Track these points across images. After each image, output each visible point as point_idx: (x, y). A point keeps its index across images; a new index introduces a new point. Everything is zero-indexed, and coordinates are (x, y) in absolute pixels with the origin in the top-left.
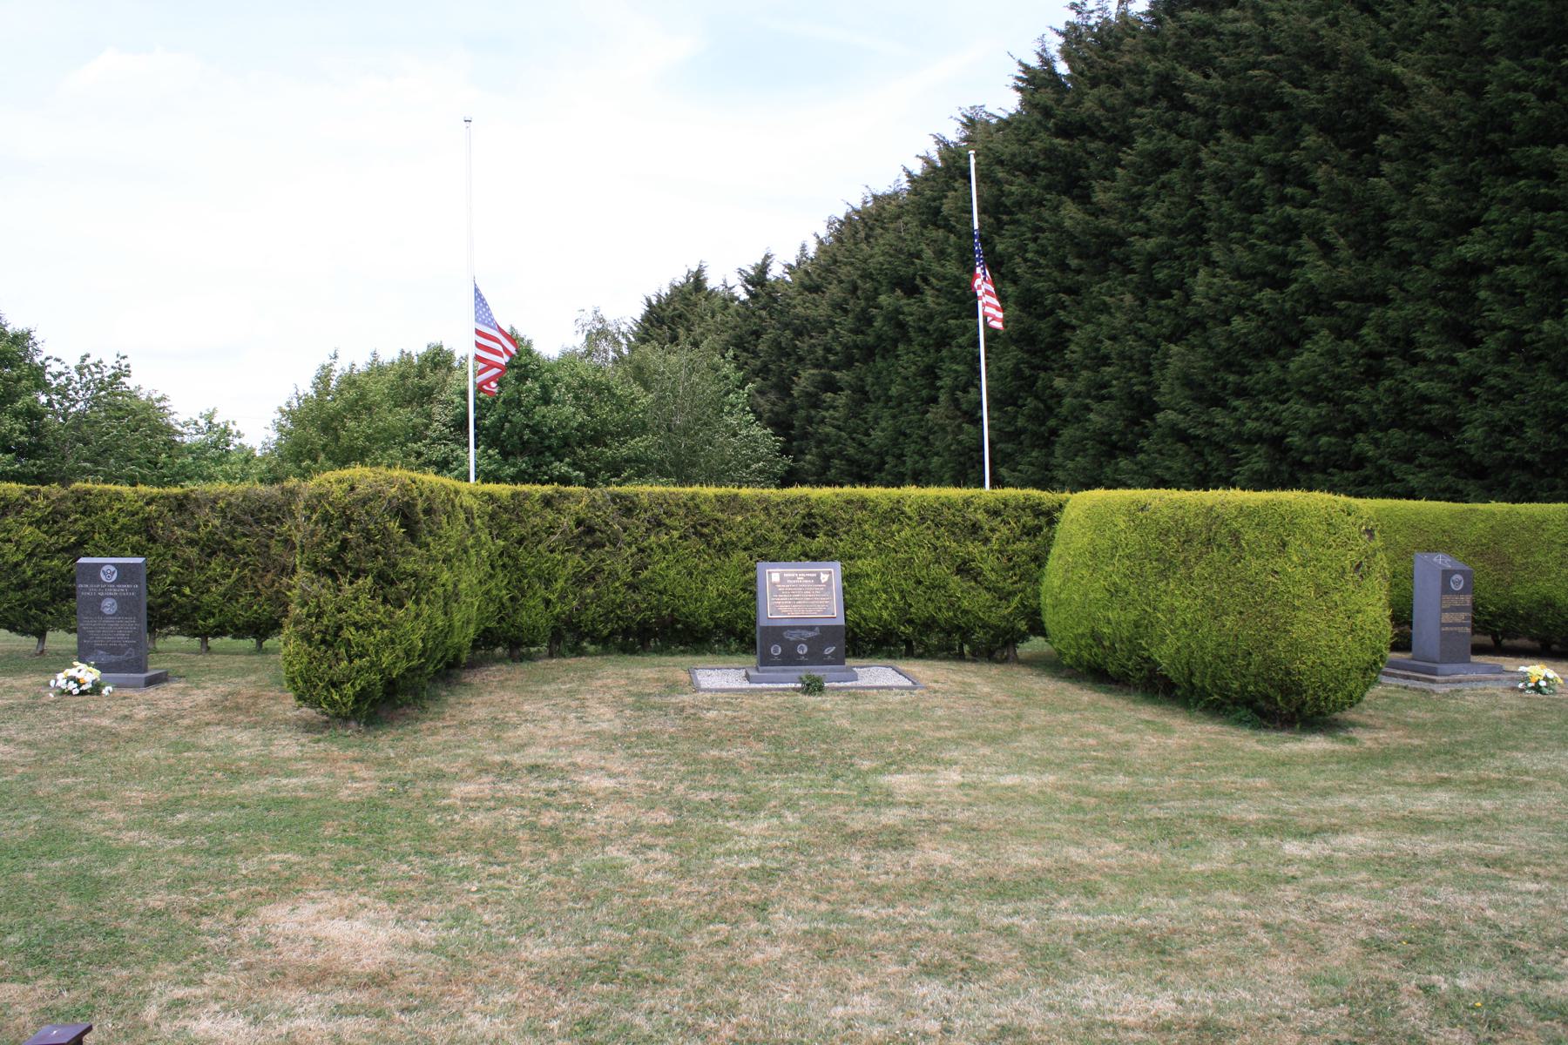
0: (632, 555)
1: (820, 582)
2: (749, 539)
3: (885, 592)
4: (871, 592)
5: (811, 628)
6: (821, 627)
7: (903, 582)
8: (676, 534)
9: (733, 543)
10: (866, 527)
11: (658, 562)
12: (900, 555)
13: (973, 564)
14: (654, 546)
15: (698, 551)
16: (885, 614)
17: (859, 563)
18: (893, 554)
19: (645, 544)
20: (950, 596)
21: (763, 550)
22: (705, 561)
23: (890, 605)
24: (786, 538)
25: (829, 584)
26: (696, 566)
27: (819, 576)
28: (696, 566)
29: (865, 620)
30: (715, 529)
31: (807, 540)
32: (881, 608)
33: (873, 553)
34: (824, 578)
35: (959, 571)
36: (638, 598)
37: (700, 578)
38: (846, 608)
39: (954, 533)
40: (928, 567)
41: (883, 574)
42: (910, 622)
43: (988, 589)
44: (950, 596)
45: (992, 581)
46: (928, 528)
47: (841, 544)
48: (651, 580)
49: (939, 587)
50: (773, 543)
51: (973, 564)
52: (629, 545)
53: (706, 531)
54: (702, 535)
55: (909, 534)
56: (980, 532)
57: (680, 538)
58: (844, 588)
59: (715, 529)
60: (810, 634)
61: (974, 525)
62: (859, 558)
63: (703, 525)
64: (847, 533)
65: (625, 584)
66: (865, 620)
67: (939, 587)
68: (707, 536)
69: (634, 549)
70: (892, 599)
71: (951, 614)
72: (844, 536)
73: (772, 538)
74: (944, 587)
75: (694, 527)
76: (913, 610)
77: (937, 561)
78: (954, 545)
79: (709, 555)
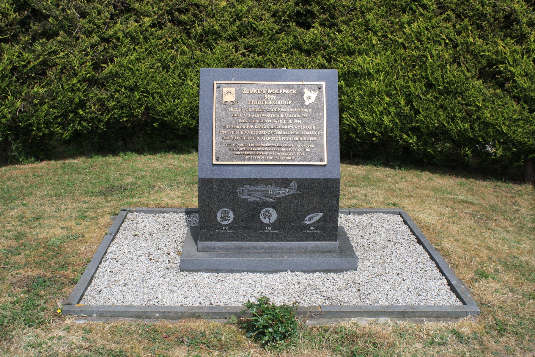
0: (92, 46)
1: (302, 105)
2: (234, 28)
3: (388, 95)
4: (372, 94)
5: (284, 183)
6: (302, 183)
7: (411, 84)
8: (147, 21)
9: (215, 33)
10: (370, 16)
11: (126, 54)
12: (409, 52)
13: (501, 67)
14: (120, 34)
15: (175, 41)
16: (386, 121)
17: (360, 59)
18: (402, 51)
19: (111, 32)
20: (468, 105)
21: (251, 41)
22: (183, 53)
23: (392, 109)
24: (277, 27)
25: (316, 107)
26: (173, 59)
27: (301, 93)
28: (173, 59)
29: (363, 124)
30: (195, 16)
31: (301, 30)
32: (381, 113)
33: (377, 48)
34: (310, 97)
35: (482, 75)
36: (103, 95)
37: (177, 72)
38: (342, 110)
39: (479, 27)
40: (442, 67)
41: (387, 73)
42: (415, 130)
43: (517, 99)
44: (468, 105)
45: (523, 90)
46: (448, 19)
47: (339, 36)
48: (116, 75)
49: (455, 94)
50: (261, 34)
51: (501, 67)
52: (89, 34)
53: (183, 17)
54: (180, 23)
55: (423, 26)
56: (515, 27)
57: (153, 25)
58: (340, 88)
59: (195, 16)
60: (282, 192)
61: (507, 17)
62: (360, 53)
63: (180, 11)
64: (346, 23)
65: (84, 80)
66: (363, 124)
67: (455, 94)
68: (186, 23)
69: (95, 38)
70: (396, 104)
71: (467, 126)
72: (343, 27)
73: (260, 28)
74: (461, 94)
75: (170, 13)
76: (421, 117)
77: (456, 61)
78: (479, 42)
79: (188, 46)
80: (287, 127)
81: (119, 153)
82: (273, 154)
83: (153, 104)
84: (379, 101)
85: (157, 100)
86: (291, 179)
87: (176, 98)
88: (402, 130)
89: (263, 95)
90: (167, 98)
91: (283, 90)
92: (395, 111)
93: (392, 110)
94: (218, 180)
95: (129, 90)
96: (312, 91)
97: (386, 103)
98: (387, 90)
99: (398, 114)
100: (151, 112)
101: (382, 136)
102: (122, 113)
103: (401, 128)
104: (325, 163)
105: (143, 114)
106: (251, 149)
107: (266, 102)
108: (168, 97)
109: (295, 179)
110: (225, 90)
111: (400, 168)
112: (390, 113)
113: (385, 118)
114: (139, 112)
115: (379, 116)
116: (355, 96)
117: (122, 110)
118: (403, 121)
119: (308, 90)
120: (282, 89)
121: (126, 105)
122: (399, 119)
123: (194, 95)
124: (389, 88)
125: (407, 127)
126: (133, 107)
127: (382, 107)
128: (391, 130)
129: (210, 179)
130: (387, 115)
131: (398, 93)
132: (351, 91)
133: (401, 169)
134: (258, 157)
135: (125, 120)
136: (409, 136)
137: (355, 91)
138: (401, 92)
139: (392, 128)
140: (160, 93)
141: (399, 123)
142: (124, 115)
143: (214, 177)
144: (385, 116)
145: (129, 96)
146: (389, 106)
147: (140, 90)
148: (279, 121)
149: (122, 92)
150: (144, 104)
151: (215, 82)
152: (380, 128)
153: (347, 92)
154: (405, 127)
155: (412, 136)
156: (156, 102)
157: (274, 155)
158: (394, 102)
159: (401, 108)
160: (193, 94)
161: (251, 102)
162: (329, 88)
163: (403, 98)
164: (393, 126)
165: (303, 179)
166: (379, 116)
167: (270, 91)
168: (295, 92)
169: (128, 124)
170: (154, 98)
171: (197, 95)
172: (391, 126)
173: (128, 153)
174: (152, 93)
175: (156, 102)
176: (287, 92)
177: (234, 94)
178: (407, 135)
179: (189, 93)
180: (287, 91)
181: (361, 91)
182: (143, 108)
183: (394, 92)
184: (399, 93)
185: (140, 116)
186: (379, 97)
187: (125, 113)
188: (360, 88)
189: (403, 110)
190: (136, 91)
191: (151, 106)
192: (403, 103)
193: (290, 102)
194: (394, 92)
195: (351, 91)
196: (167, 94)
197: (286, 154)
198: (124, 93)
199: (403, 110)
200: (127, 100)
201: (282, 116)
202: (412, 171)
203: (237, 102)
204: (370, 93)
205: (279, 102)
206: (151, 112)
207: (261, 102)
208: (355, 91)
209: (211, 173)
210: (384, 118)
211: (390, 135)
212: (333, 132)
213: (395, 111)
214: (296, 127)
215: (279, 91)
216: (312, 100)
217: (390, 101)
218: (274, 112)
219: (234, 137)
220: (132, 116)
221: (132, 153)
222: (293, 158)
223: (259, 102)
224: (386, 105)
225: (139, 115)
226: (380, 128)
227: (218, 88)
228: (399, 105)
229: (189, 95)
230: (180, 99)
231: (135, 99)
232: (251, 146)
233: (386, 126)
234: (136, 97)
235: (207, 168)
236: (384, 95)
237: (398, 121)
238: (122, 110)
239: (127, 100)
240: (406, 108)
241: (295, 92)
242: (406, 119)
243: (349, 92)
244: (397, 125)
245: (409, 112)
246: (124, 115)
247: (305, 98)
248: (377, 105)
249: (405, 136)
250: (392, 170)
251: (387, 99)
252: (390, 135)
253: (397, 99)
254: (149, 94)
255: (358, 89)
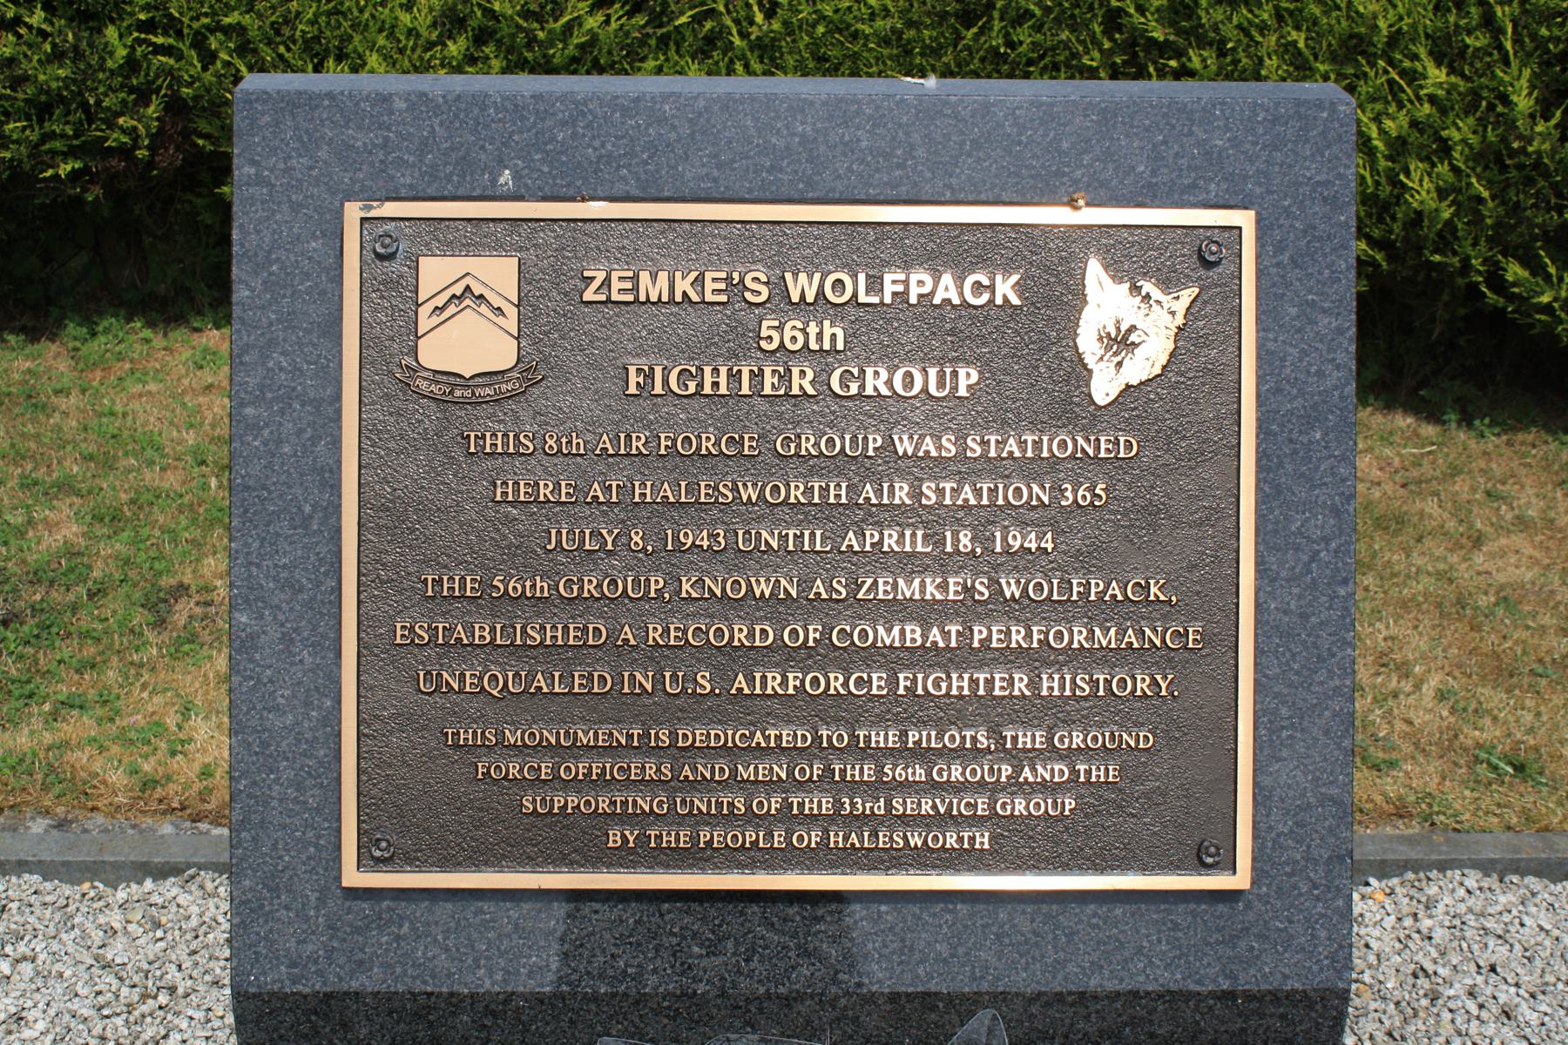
3: (1447, 52)
23: (1461, 132)
80: (944, 587)
81: (60, 324)
82: (827, 807)
83: (208, 91)
84: (1391, 82)
85: (228, 64)
86: (964, 997)
87: (327, 51)
88: (1504, 242)
89: (750, 318)
90: (281, 56)
91: (914, 278)
92: (1474, 140)
93: (1456, 136)
94: (388, 1003)
95: (71, 20)
96: (1148, 287)
97: (1432, 99)
98: (1436, 30)
99: (1491, 159)
100: (203, 126)
101: (1390, 258)
102: (47, 137)
103: (1498, 225)
104: (1240, 880)
105: (158, 140)
106: (650, 772)
107: (769, 380)
108: (282, 49)
109: (998, 999)
110: (436, 273)
111: (1467, 421)
112: (1445, 148)
113: (1416, 176)
114: (135, 128)
115: (1383, 164)
116: (1263, 52)
117: (41, 121)
118: (1512, 194)
119: (1117, 279)
120: (907, 266)
121: (60, 95)
122: (1490, 184)
123: (418, 36)
124: (1452, 19)
125: (1532, 225)
126: (98, 103)
127: (1403, 119)
128: (1440, 234)
129: (329, 996)
130: (1427, 159)
131: (1500, 47)
132: (1239, 27)
133: (1470, 425)
134: (704, 836)
135: (65, 169)
136: (1536, 269)
137: (1263, 28)
138: (1517, 41)
139: (1449, 223)
140: (240, 29)
141: (1490, 204)
142: (58, 145)
143: (355, 985)
144: (1416, 166)
145: (76, 48)
146: (1443, 111)
147: (132, 14)
148: (872, 536)
149: (30, 27)
150: (157, 91)
151: (353, 212)
152: (1381, 220)
153: (1216, 30)
154: (1519, 224)
155: (1552, 270)
156: (219, 76)
157: (831, 819)
158: (1476, 95)
159: (1511, 125)
160: (410, 32)
161: (650, 376)
162: (1280, 249)
163: (1527, 73)
164: (1453, 215)
165: (1059, 997)
166: (1383, 164)
167: (802, 285)
168: (1006, 288)
169: (85, 190)
170: (208, 58)
171: (434, 37)
172: (1446, 215)
173: (105, 323)
174: (197, 33)
175: (219, 76)
176: (946, 289)
177: (512, 312)
178: (1524, 264)
179: (393, 27)
180: (947, 279)
181: (1298, 28)
182: (152, 110)
183: (1476, 41)
184: (1508, 45)
185: (141, 153)
186: (1391, 62)
187: (63, 136)
188: (1291, 13)
189: (1520, 137)
190: (112, 21)
191: (196, 98)
192: (1523, 102)
193: (967, 377)
194: (1476, 41)
195: (1239, 27)
196: (278, 32)
197: (926, 808)
198: (44, 34)
199: (1520, 137)
200: (62, 73)
201: (902, 493)
202: (1530, 438)
203: (528, 373)
204: (1343, 43)
205: (876, 381)
206: (203, 126)
207: (735, 377)
208: (1263, 28)
209: (330, 952)
210: (1408, 174)
211: (1437, 258)
212: (1304, 616)
213: (1474, 140)
214: (1011, 590)
215: (875, 284)
216: (1144, 364)
217: (1454, 86)
218: (839, 465)
219: (507, 678)
220: (95, 149)
221: (129, 320)
222: (983, 840)
223: (716, 379)
224: (1427, 108)
225: (136, 146)
226: (1381, 220)
227: (380, 257)
228: (1500, 109)
229: (391, 35)
230: (347, 56)
231: (110, 64)
232: (646, 749)
233: (1419, 214)
234: (111, 54)
235: (302, 916)
236: (1422, 52)
237: (1486, 194)
238: (41, 121)
239: (62, 73)
240: (1540, 128)
241: (1006, 288)
242: (1530, 181)
243: (1229, 31)
244: (1477, 213)
245: (1554, 151)
246: (58, 145)
247: (1088, 343)
248: (1378, 106)
249: (1514, 271)
250: (1429, 430)
251: (1437, 75)
252: (1437, 258)
253: (1494, 77)
254: (179, 35)
255: (1279, 17)
